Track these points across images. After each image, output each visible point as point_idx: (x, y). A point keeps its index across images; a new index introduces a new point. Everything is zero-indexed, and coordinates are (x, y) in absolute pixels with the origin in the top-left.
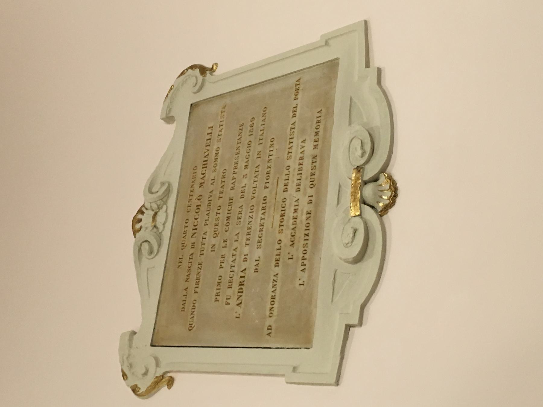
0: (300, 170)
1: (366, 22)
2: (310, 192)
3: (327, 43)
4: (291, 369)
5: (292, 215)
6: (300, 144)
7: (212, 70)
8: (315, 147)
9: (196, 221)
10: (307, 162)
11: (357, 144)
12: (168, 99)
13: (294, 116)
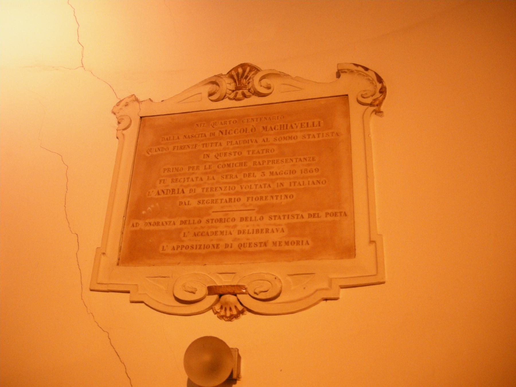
0: (257, 231)
1: (383, 283)
2: (235, 245)
3: (371, 242)
4: (104, 252)
5: (219, 229)
6: (281, 227)
7: (378, 112)
8: (274, 244)
9: (233, 132)
10: (262, 237)
11: (266, 286)
12: (355, 68)
13: (310, 216)
